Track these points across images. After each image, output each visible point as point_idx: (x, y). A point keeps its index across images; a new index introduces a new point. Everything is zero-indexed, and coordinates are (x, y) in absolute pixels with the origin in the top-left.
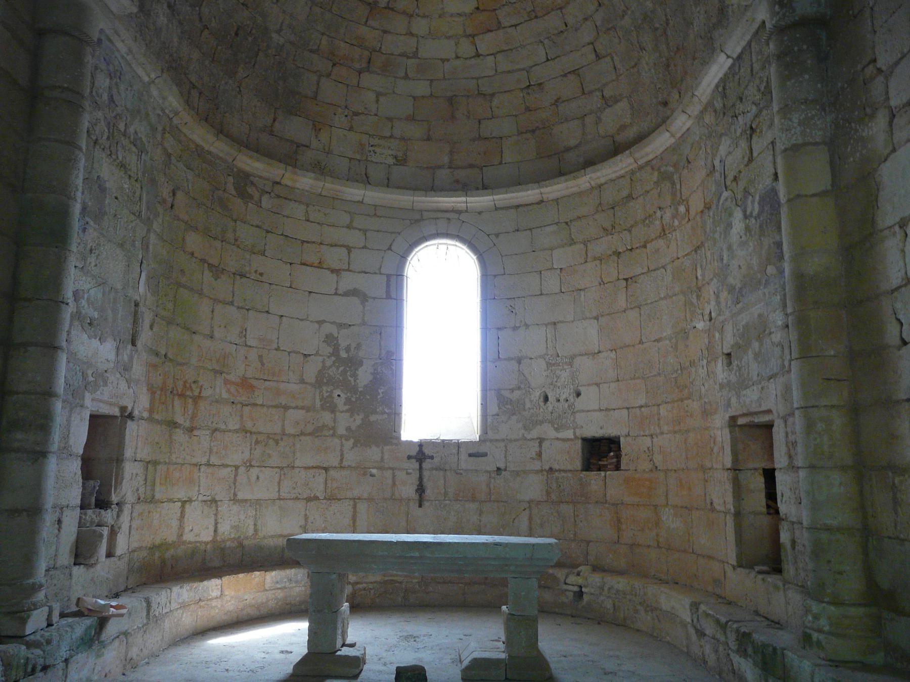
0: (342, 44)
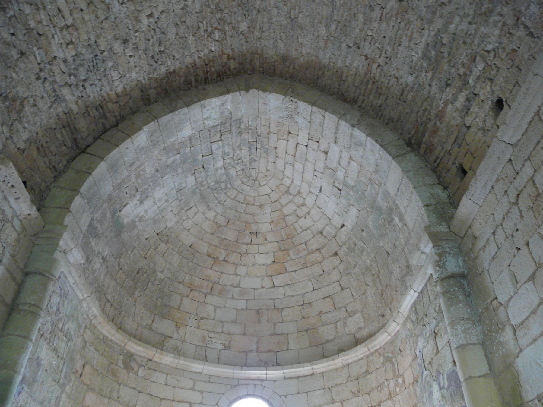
0: (197, 279)
